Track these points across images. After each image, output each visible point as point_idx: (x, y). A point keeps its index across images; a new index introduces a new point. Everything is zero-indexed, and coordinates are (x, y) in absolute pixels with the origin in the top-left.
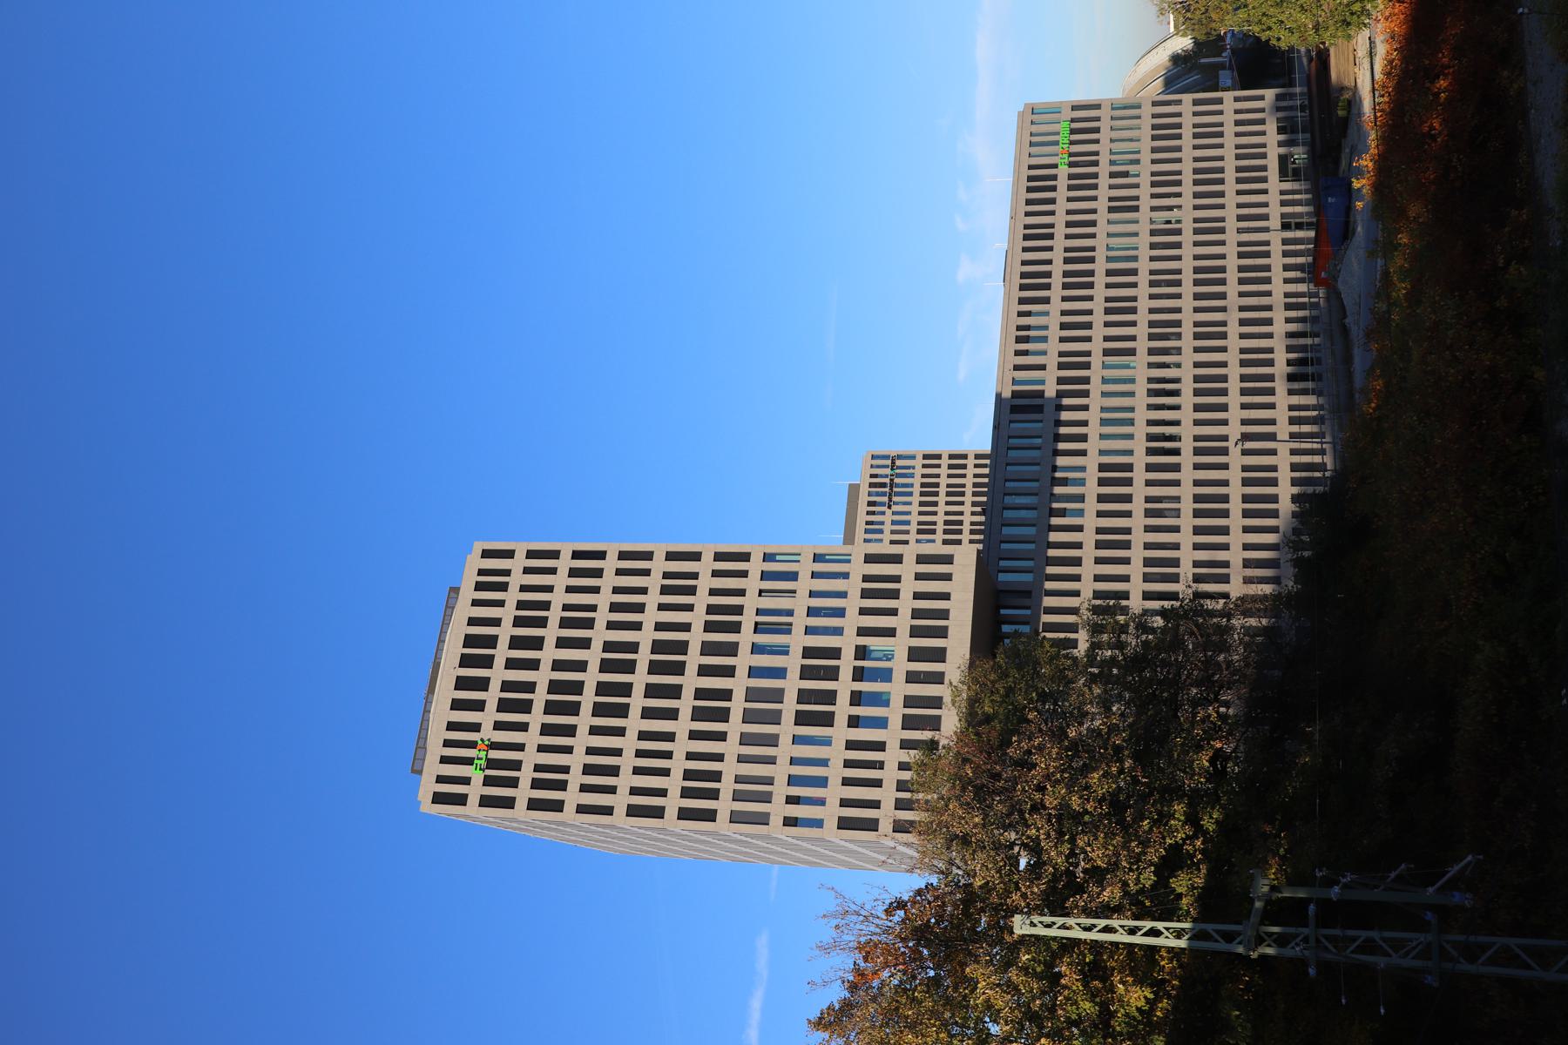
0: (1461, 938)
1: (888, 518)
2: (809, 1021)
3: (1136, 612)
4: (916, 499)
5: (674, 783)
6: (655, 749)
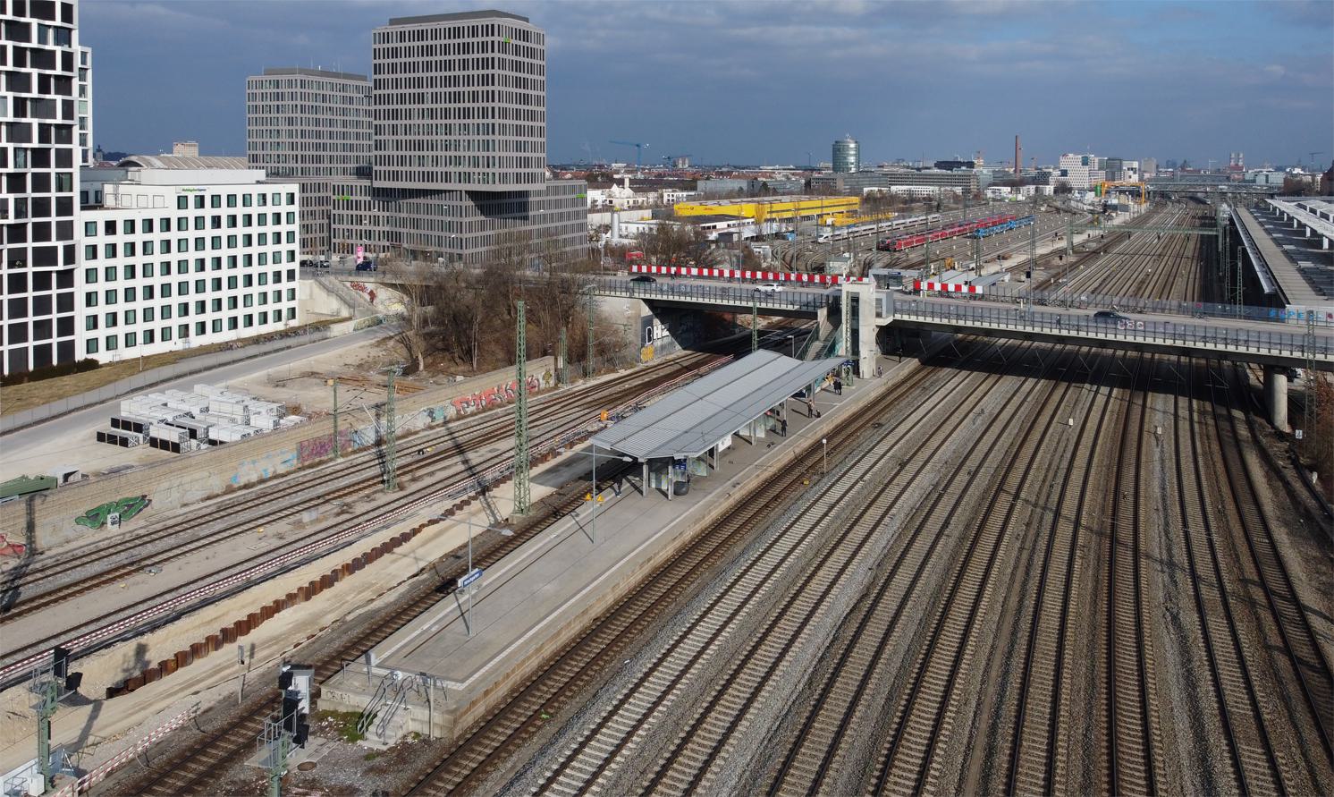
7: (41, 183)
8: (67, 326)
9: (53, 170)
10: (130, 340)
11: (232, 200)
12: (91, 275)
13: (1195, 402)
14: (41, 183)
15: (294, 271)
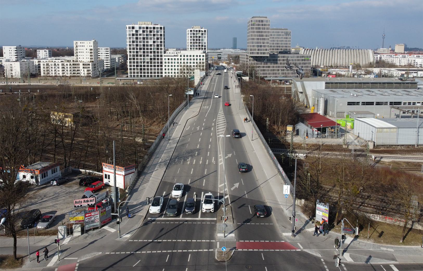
0: (249, 73)
1: (283, 34)
2: (395, 114)
3: (370, 148)
4: (285, 37)
5: (253, 37)
6: (255, 36)
7: (158, 52)
8: (162, 73)
9: (160, 51)
10: (131, 69)
11: (190, 56)
12: (165, 66)
13: (321, 112)
14: (158, 52)
15: (62, 64)
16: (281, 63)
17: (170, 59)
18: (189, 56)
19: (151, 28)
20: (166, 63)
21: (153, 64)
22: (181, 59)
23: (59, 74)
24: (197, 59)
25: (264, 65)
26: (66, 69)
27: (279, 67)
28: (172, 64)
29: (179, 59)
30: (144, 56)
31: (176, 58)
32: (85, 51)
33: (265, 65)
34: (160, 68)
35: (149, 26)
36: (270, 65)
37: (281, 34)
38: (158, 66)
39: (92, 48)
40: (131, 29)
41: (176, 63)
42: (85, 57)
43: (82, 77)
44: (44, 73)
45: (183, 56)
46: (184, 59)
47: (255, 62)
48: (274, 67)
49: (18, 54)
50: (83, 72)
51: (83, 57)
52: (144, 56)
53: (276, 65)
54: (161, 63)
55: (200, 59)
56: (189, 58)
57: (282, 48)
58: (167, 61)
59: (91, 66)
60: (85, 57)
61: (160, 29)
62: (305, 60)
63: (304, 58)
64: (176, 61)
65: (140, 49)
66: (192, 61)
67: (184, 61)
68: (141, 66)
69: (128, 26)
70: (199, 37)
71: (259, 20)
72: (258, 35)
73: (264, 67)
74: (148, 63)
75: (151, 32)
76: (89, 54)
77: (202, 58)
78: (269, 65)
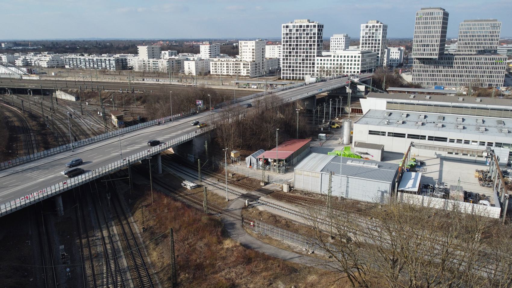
9: (312, 51)
16: (458, 67)
17: (323, 60)
18: (343, 57)
19: (304, 26)
20: (318, 64)
21: (305, 65)
22: (334, 60)
23: (224, 72)
24: (351, 61)
25: (434, 69)
26: (230, 68)
27: (455, 72)
28: (348, 62)
29: (333, 60)
30: (297, 56)
31: (329, 58)
32: (248, 51)
33: (435, 69)
34: (312, 69)
35: (303, 24)
36: (442, 69)
37: (486, 27)
38: (310, 67)
39: (254, 48)
40: (285, 28)
41: (329, 64)
42: (248, 57)
43: (242, 76)
44: (213, 72)
45: (336, 57)
46: (337, 60)
47: (422, 65)
48: (447, 71)
49: (211, 52)
50: (244, 73)
51: (246, 56)
52: (297, 56)
53: (451, 69)
54: (313, 64)
55: (331, 64)
56: (343, 59)
57: (485, 45)
58: (319, 62)
59: (250, 66)
60: (248, 57)
61: (314, 27)
62: (496, 64)
63: (495, 61)
64: (329, 62)
65: (293, 49)
66: (346, 62)
67: (337, 62)
68: (293, 67)
69: (283, 25)
70: (373, 33)
71: (427, 12)
72: (424, 31)
73: (433, 71)
74: (300, 63)
75: (304, 30)
76: (252, 54)
77: (357, 59)
78: (441, 69)
